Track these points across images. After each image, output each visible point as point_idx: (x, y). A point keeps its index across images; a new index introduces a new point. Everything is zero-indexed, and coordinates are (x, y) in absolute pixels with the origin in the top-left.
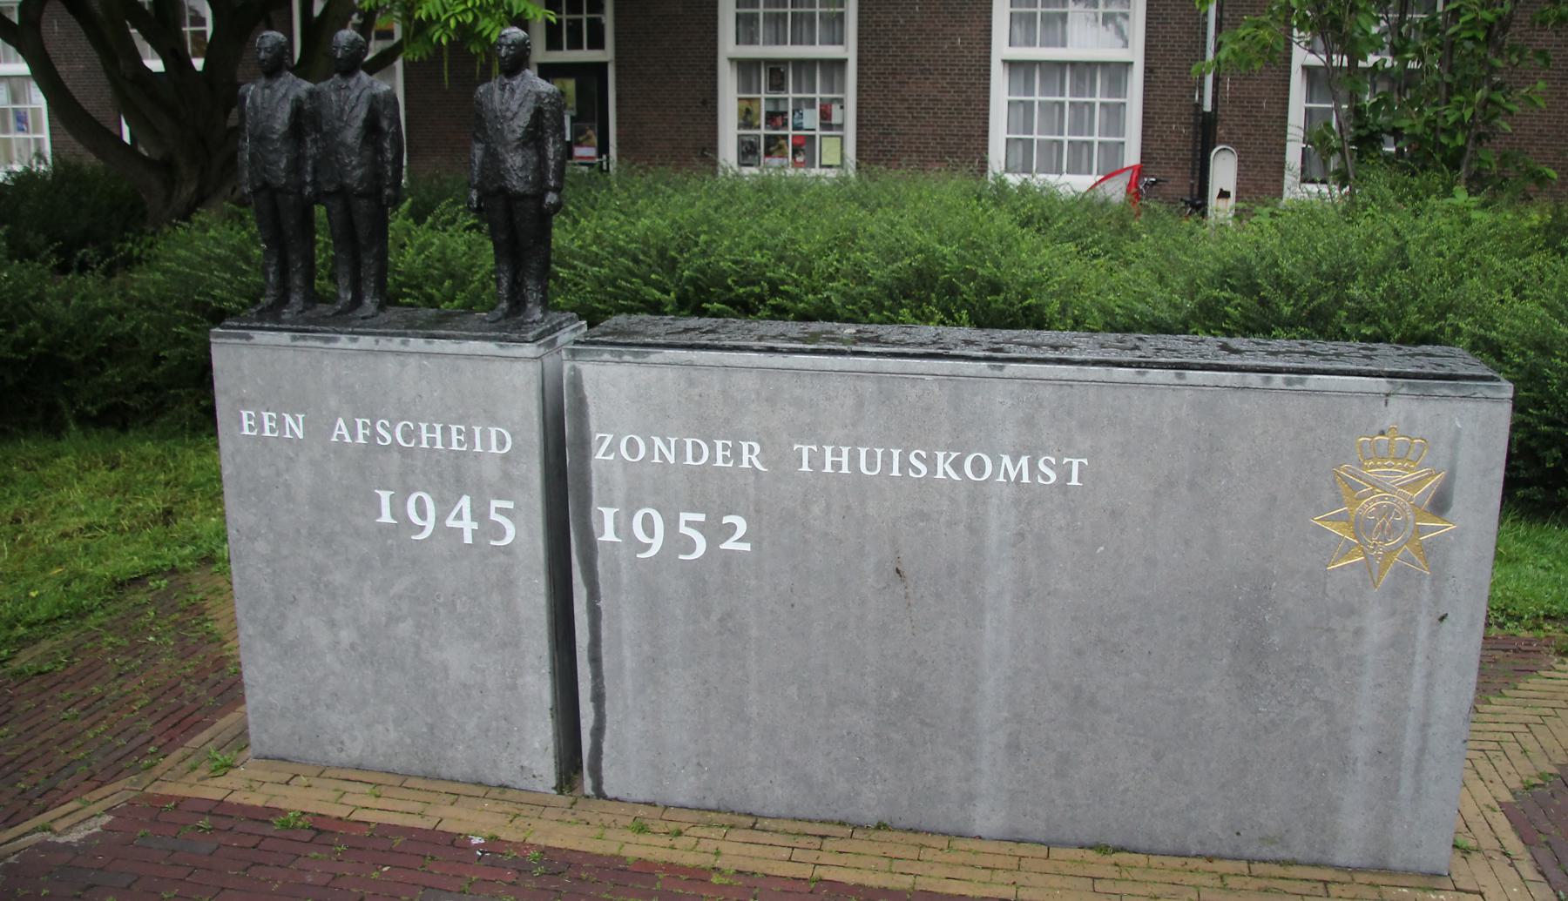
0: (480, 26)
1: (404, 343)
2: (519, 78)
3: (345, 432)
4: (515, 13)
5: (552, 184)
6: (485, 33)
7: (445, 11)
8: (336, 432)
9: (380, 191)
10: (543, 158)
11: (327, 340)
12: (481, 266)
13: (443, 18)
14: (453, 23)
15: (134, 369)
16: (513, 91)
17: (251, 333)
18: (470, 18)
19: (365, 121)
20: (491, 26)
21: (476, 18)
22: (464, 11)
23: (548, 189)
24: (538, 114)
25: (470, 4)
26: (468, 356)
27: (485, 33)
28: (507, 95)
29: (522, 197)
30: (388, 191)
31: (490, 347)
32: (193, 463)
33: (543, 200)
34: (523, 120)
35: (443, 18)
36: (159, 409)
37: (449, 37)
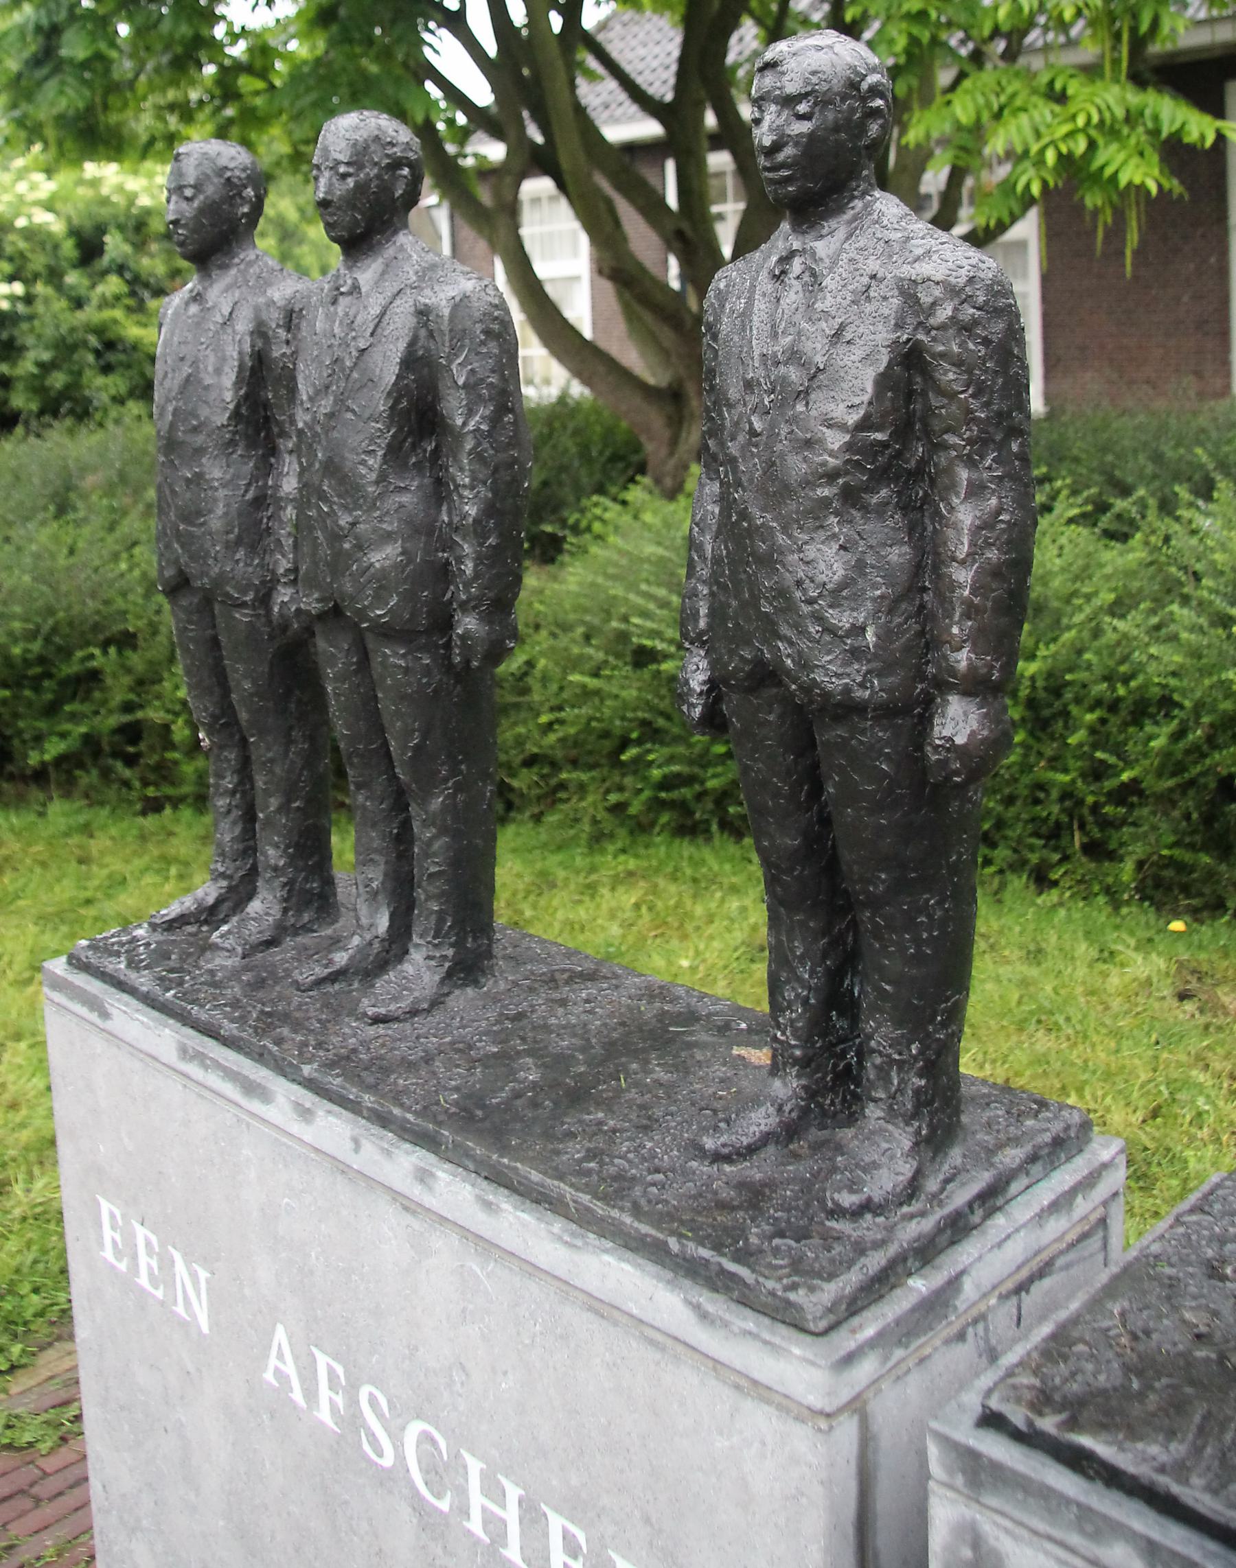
0: (1100, 159)
1: (423, 1176)
2: (837, 227)
3: (290, 1369)
4: (1165, 134)
5: (962, 659)
6: (1108, 171)
7: (1038, 135)
8: (273, 1361)
9: (444, 623)
10: (928, 560)
11: (251, 1088)
12: (1088, 597)
13: (1035, 148)
14: (1050, 157)
15: (521, 730)
16: (814, 281)
17: (117, 1003)
18: (1081, 146)
19: (397, 392)
20: (1121, 156)
21: (1092, 145)
22: (1070, 135)
23: (942, 686)
24: (909, 368)
25: (1081, 121)
26: (600, 1308)
27: (1108, 171)
28: (793, 296)
29: (846, 709)
30: (468, 623)
31: (662, 1300)
32: (560, 915)
33: (925, 722)
34: (849, 396)
35: (1035, 148)
36: (552, 795)
37: (1045, 183)
